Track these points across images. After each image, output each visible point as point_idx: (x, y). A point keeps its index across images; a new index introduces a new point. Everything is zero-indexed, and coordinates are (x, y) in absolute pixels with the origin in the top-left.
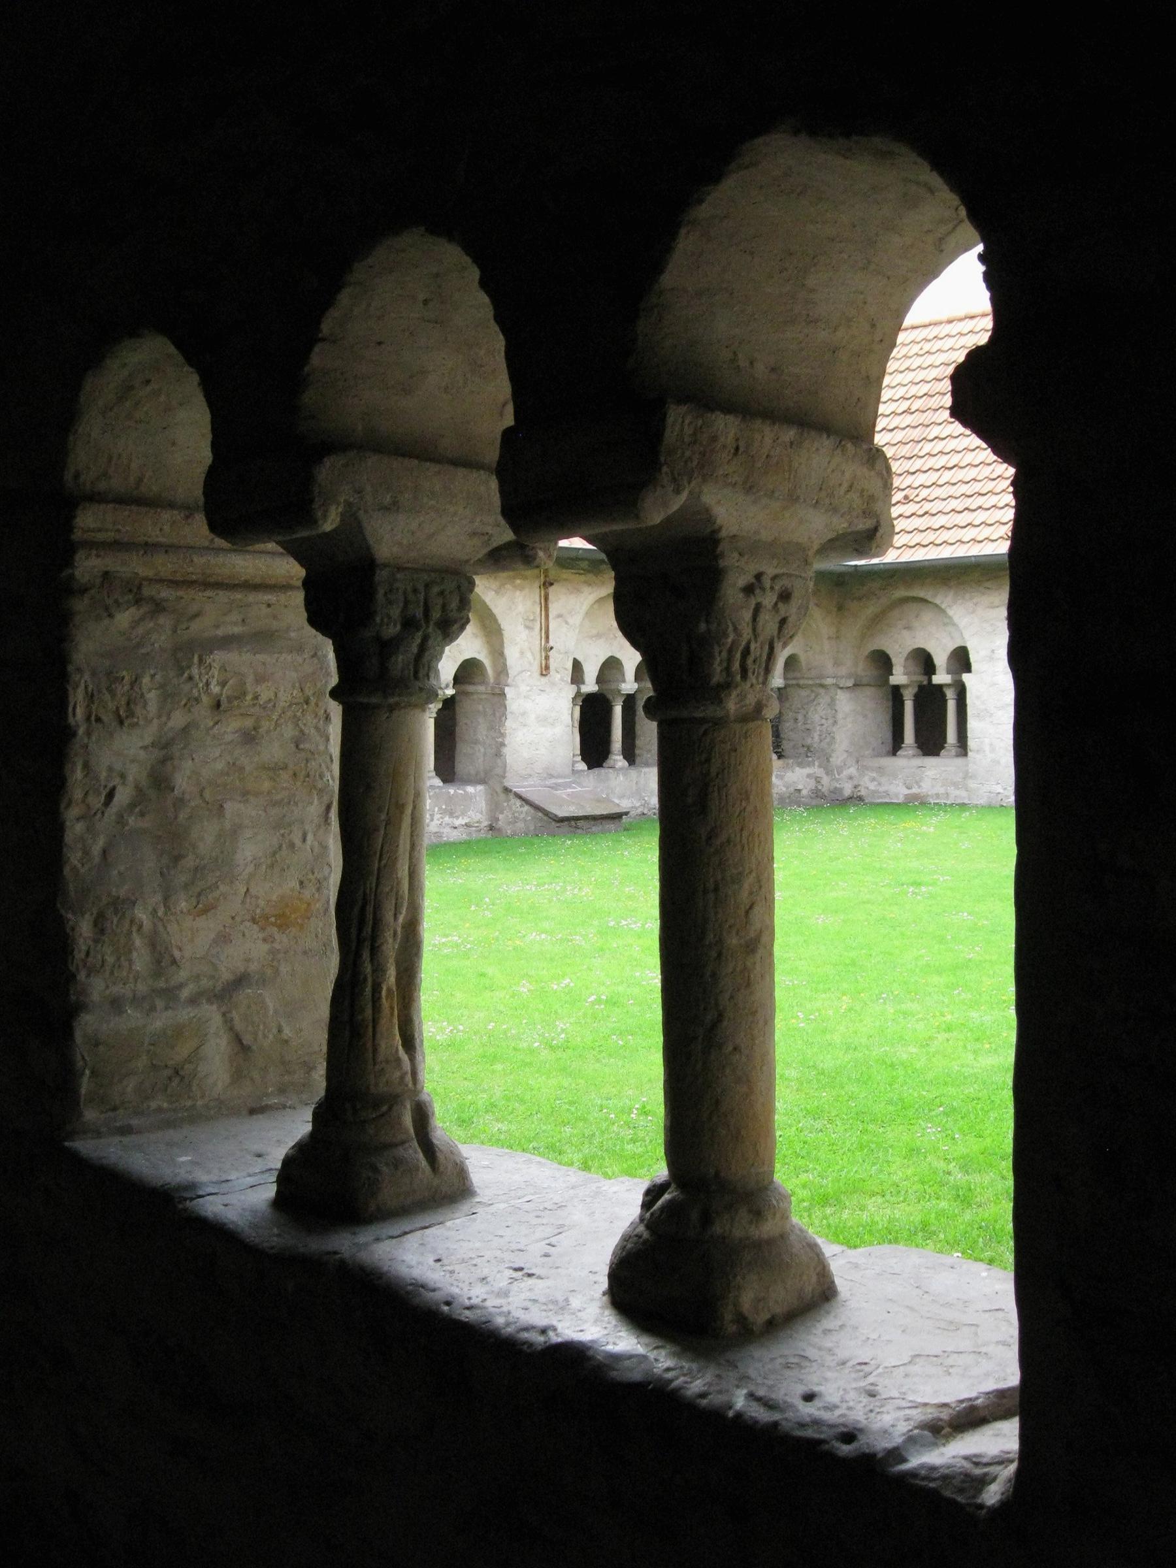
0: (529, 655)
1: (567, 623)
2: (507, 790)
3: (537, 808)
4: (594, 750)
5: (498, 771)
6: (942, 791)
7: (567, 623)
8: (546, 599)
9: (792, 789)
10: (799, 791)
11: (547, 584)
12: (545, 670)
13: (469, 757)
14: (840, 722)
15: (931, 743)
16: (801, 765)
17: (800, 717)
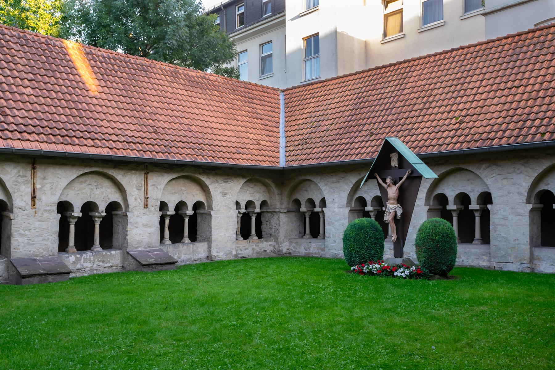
0: (139, 200)
1: (157, 188)
2: (128, 253)
3: (137, 260)
4: (244, 232)
5: (125, 245)
6: (317, 252)
7: (157, 188)
8: (147, 178)
9: (263, 250)
10: (266, 251)
11: (147, 174)
12: (146, 206)
13: (117, 239)
14: (282, 225)
15: (193, 238)
16: (266, 241)
17: (268, 223)
